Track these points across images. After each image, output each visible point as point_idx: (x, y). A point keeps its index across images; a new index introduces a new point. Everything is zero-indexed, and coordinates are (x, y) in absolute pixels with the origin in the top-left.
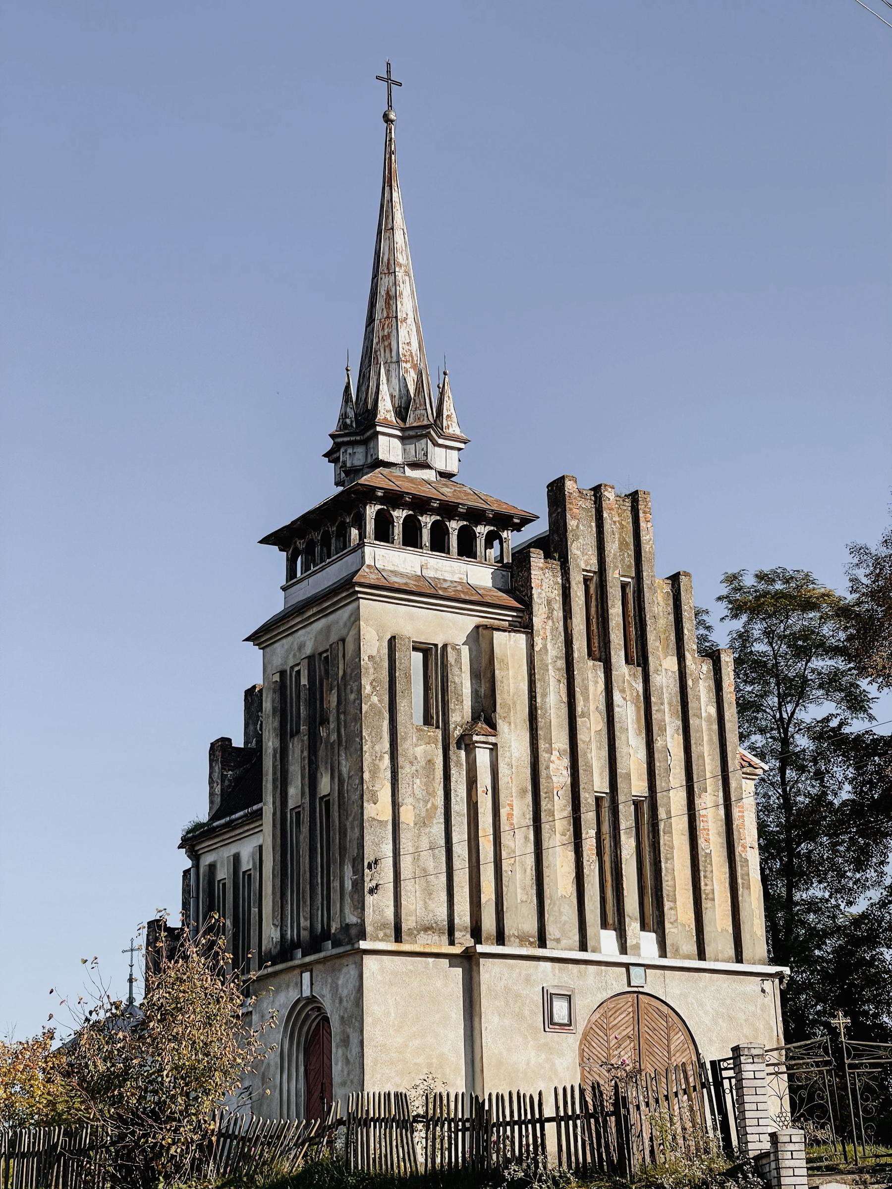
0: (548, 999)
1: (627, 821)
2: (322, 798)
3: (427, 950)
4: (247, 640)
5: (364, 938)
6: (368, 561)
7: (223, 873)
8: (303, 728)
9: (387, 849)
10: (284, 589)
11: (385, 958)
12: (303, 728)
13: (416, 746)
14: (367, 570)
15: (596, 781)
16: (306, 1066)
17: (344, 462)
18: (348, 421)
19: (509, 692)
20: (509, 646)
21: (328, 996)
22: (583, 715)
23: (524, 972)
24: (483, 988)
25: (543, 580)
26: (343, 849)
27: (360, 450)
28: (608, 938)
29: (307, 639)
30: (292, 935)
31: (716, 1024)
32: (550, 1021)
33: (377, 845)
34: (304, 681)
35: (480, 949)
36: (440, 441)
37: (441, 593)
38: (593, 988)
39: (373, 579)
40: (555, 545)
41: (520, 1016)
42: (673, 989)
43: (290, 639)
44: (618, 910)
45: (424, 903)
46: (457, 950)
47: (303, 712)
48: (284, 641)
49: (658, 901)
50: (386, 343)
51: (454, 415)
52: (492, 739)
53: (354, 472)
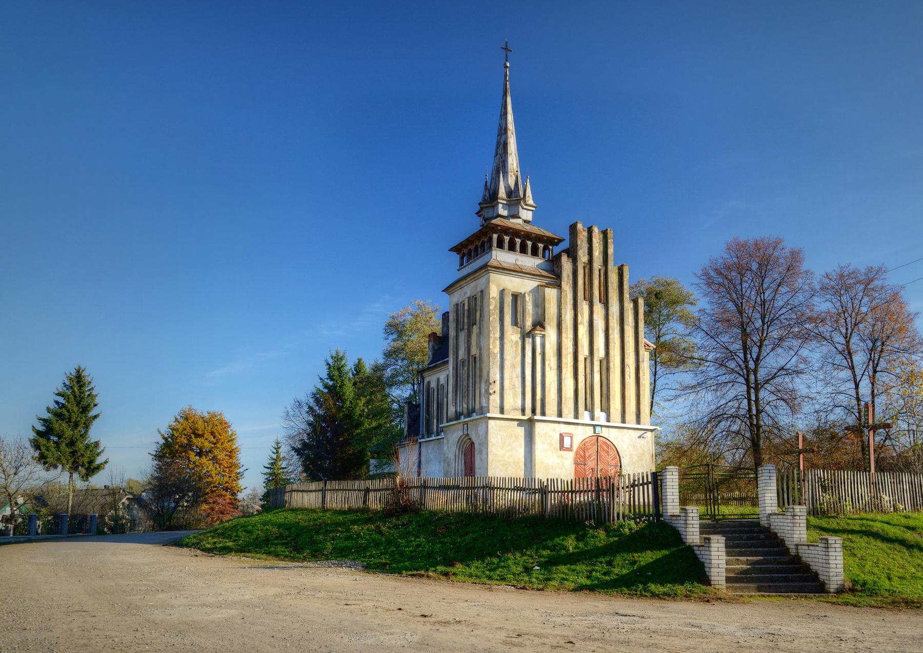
6: (494, 257)
8: (466, 327)
9: (498, 377)
11: (498, 421)
12: (466, 327)
15: (584, 351)
20: (551, 294)
24: (537, 433)
25: (566, 265)
26: (481, 376)
27: (490, 210)
28: (587, 414)
29: (468, 290)
32: (562, 447)
33: (495, 375)
34: (466, 307)
35: (536, 417)
38: (581, 434)
40: (572, 253)
41: (551, 444)
42: (612, 435)
45: (513, 400)
46: (525, 418)
47: (466, 321)
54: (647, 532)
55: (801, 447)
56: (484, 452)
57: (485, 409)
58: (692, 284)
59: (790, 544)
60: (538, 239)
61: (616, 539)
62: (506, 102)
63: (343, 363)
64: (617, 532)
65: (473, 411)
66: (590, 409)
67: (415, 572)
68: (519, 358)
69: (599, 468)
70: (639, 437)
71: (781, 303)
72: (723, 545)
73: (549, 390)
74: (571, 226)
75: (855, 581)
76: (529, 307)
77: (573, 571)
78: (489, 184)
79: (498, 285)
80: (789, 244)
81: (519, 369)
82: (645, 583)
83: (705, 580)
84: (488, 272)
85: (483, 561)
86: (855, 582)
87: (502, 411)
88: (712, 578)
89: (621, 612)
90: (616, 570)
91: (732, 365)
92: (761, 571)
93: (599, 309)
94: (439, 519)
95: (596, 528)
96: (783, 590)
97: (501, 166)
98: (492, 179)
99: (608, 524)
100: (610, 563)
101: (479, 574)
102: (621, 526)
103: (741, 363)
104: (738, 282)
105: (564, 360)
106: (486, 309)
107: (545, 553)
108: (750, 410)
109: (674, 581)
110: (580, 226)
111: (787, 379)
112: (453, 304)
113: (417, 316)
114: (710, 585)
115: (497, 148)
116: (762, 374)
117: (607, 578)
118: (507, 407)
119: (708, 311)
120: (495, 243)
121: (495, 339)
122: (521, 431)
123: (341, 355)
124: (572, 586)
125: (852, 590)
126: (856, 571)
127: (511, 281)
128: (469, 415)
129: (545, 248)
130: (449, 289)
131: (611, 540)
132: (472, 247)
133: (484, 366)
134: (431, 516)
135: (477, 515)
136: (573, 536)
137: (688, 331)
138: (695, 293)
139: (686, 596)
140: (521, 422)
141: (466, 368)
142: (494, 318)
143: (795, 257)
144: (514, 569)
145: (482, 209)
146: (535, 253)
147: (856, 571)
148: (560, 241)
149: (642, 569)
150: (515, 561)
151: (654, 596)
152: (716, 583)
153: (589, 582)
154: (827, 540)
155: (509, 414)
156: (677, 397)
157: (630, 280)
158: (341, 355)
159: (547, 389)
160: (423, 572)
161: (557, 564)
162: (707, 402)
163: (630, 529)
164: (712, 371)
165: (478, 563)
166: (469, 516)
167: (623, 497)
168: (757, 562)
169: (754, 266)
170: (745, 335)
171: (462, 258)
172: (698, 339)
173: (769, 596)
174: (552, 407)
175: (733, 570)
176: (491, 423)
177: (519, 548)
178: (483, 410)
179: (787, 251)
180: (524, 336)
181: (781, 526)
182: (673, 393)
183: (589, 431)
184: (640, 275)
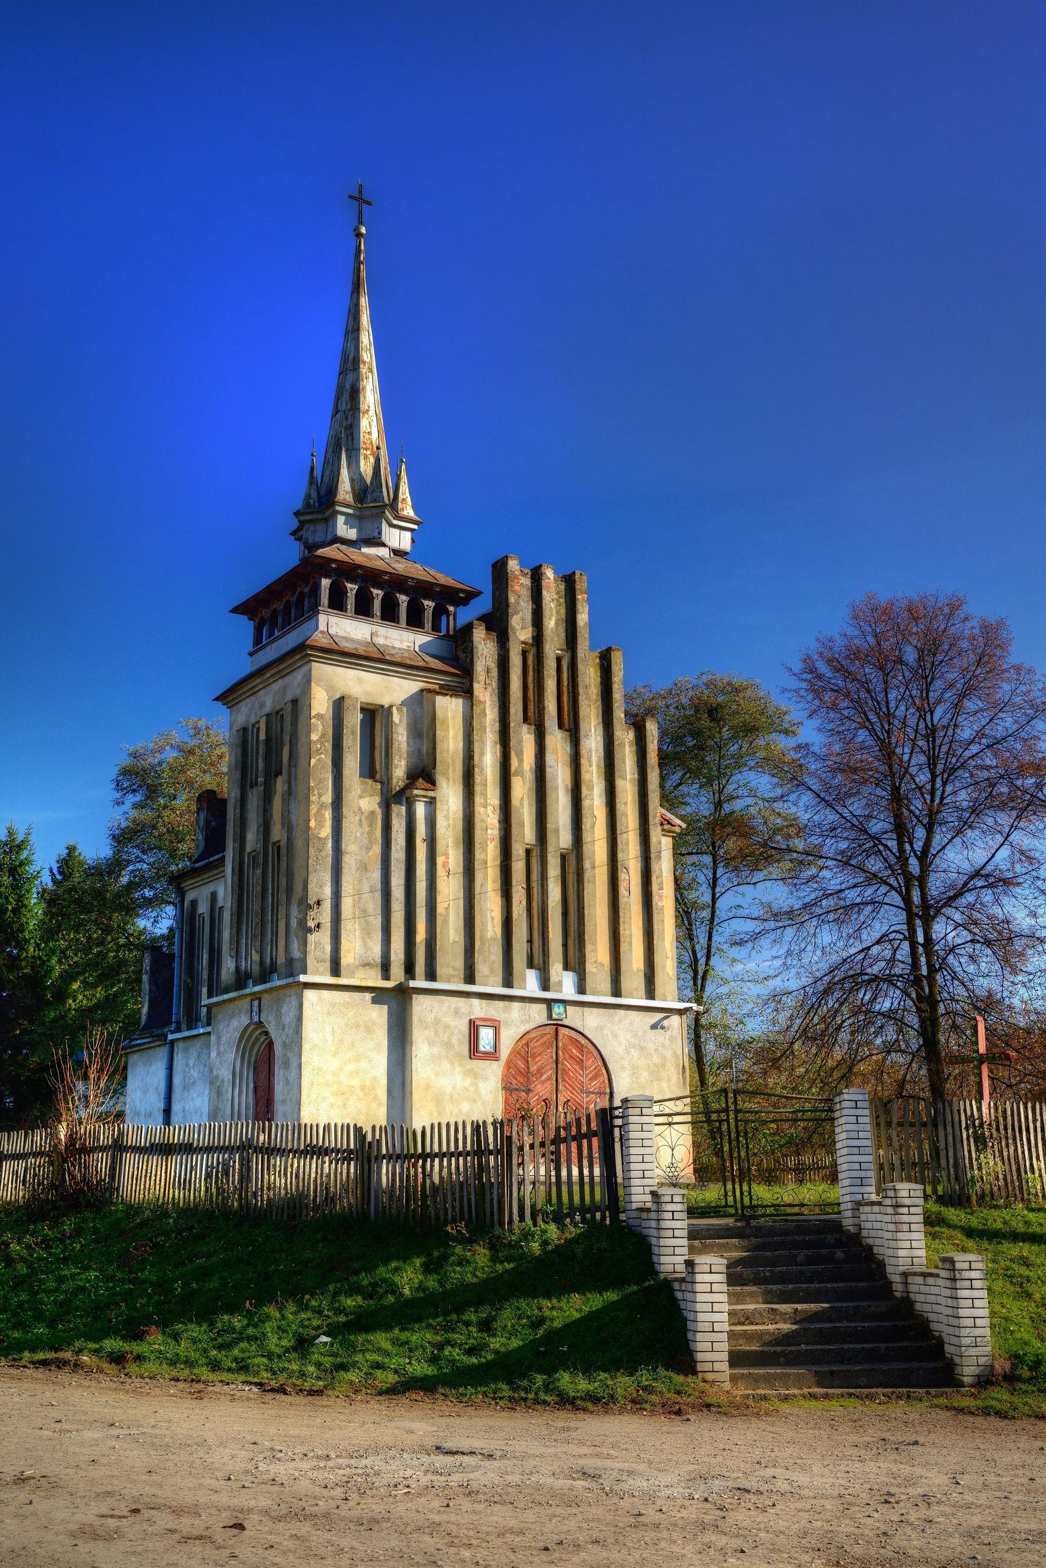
0: (474, 1028)
1: (554, 871)
2: (274, 844)
3: (363, 984)
4: (216, 699)
5: (305, 972)
6: (322, 627)
7: (203, 908)
8: (261, 779)
9: (328, 891)
10: (251, 654)
11: (325, 994)
12: (261, 779)
13: (361, 797)
14: (320, 635)
15: (525, 833)
16: (255, 1083)
17: (307, 539)
18: (312, 502)
19: (448, 751)
21: (273, 1023)
22: (517, 774)
23: (453, 1006)
24: (415, 1019)
26: (289, 891)
27: (320, 527)
30: (246, 967)
31: (628, 1053)
32: (474, 1051)
33: (320, 886)
34: (262, 736)
35: (412, 984)
36: (395, 522)
37: (388, 658)
38: (518, 1021)
39: (323, 641)
40: (497, 623)
41: (448, 1045)
42: (590, 1022)
43: (252, 698)
44: (544, 951)
45: (360, 945)
46: (389, 984)
48: (248, 700)
49: (580, 942)
50: (349, 432)
51: (409, 499)
52: (431, 794)
53: (312, 547)
54: (579, 1250)
55: (982, 1048)
56: (294, 1064)
57: (297, 965)
58: (784, 690)
59: (894, 1275)
60: (420, 589)
61: (509, 1266)
62: (357, 305)
63: (24, 855)
64: (514, 1251)
65: (273, 969)
66: (539, 963)
67: (50, 1355)
68: (377, 849)
69: (562, 1099)
70: (654, 1027)
71: (966, 734)
72: (722, 1278)
73: (446, 922)
74: (495, 566)
75: (1017, 1356)
76: (401, 737)
77: (403, 1344)
78: (318, 473)
79: (330, 689)
80: (980, 608)
81: (376, 875)
82: (550, 1371)
83: (682, 1359)
84: (307, 660)
85: (212, 1324)
86: (1016, 1358)
87: (336, 969)
88: (699, 1357)
89: (449, 1445)
90: (496, 1343)
91: (875, 865)
92: (821, 1336)
93: (557, 741)
94: (143, 1225)
95: (471, 1241)
96: (863, 1380)
97: (345, 436)
98: (326, 462)
99: (498, 1231)
100: (486, 1326)
101: (193, 1356)
102: (527, 1236)
103: (893, 860)
104: (880, 687)
105: (478, 855)
106: (302, 740)
107: (349, 1302)
108: (915, 965)
109: (612, 1366)
110: (513, 565)
111: (987, 896)
112: (235, 728)
113: (191, 752)
114: (694, 1372)
115: (338, 398)
116: (936, 885)
117: (474, 1360)
118: (347, 959)
119: (815, 749)
120: (325, 599)
121: (322, 806)
122: (379, 1015)
123: (20, 837)
124: (392, 1378)
125: (1011, 1379)
126: (1025, 1333)
127: (360, 680)
128: (264, 978)
129: (439, 612)
130: (228, 697)
131: (499, 1268)
132: (279, 605)
133: (297, 866)
134: (128, 1215)
135: (226, 1212)
136: (418, 1262)
137: (779, 792)
138: (795, 711)
139: (634, 1402)
140: (379, 995)
141: (259, 872)
142: (321, 760)
143: (992, 638)
144: (273, 1342)
145: (302, 523)
146: (415, 621)
147: (1025, 1333)
148: (471, 595)
149: (554, 1337)
150: (280, 1323)
151: (567, 1402)
152: (708, 1367)
153: (430, 1370)
154: (952, 1261)
155: (352, 974)
156: (756, 936)
157: (625, 682)
158: (20, 837)
159: (439, 920)
160: (67, 1355)
161: (369, 1328)
162: (826, 946)
163: (545, 1243)
164: (833, 878)
165: (197, 1330)
166: (209, 1214)
167: (534, 1170)
168: (816, 1317)
169: (910, 655)
170: (897, 799)
171: (258, 630)
172: (801, 808)
173: (826, 1396)
174: (450, 961)
175: (747, 1336)
176: (310, 995)
177: (295, 1291)
178: (296, 966)
179: (974, 623)
180: (389, 799)
181: (875, 1225)
182: (750, 926)
183: (537, 1014)
184: (685, 668)
